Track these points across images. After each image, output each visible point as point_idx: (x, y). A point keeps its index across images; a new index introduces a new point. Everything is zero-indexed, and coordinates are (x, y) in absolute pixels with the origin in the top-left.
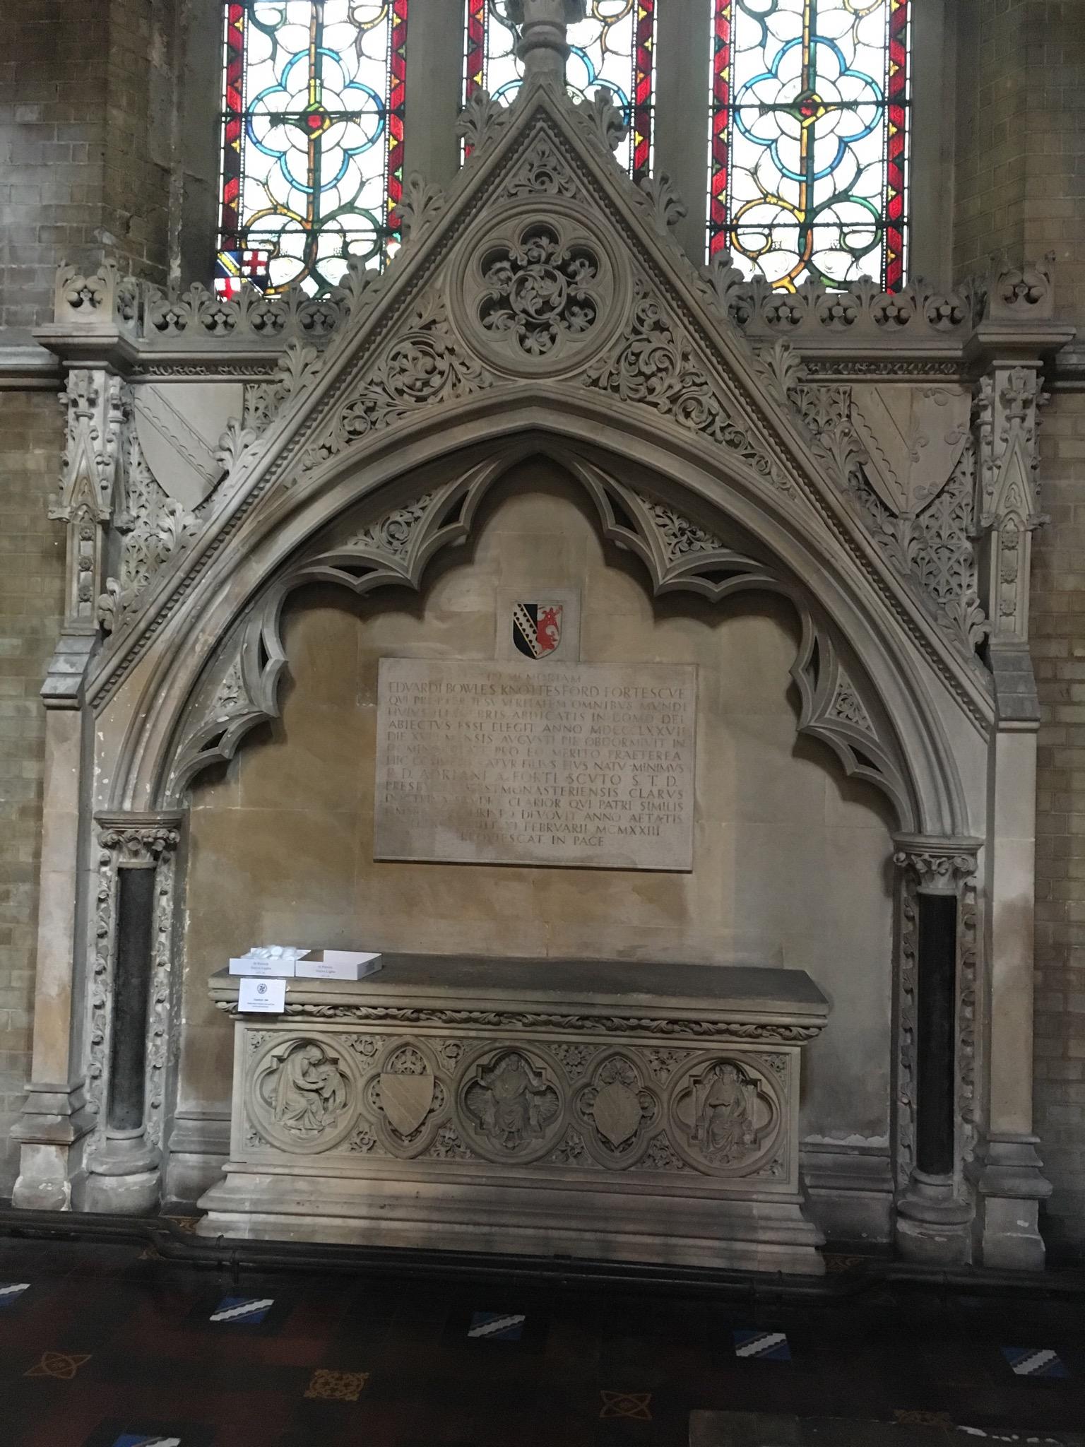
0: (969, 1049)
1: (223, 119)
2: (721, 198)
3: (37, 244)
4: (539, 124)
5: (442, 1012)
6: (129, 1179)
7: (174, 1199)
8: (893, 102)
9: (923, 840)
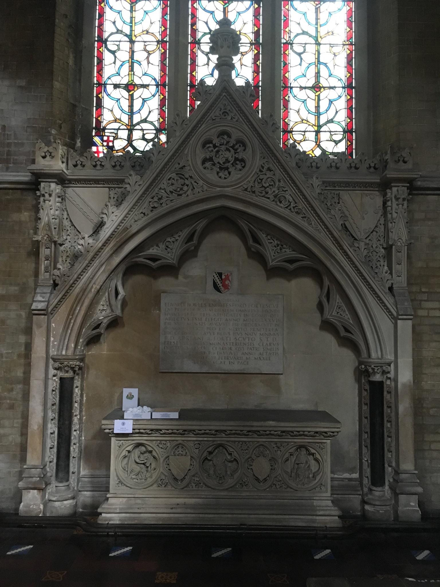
0: (389, 439)
1: (95, 85)
2: (286, 120)
3: (25, 133)
4: (224, 94)
5: (194, 431)
6: (65, 502)
7: (81, 510)
8: (349, 87)
9: (371, 360)
